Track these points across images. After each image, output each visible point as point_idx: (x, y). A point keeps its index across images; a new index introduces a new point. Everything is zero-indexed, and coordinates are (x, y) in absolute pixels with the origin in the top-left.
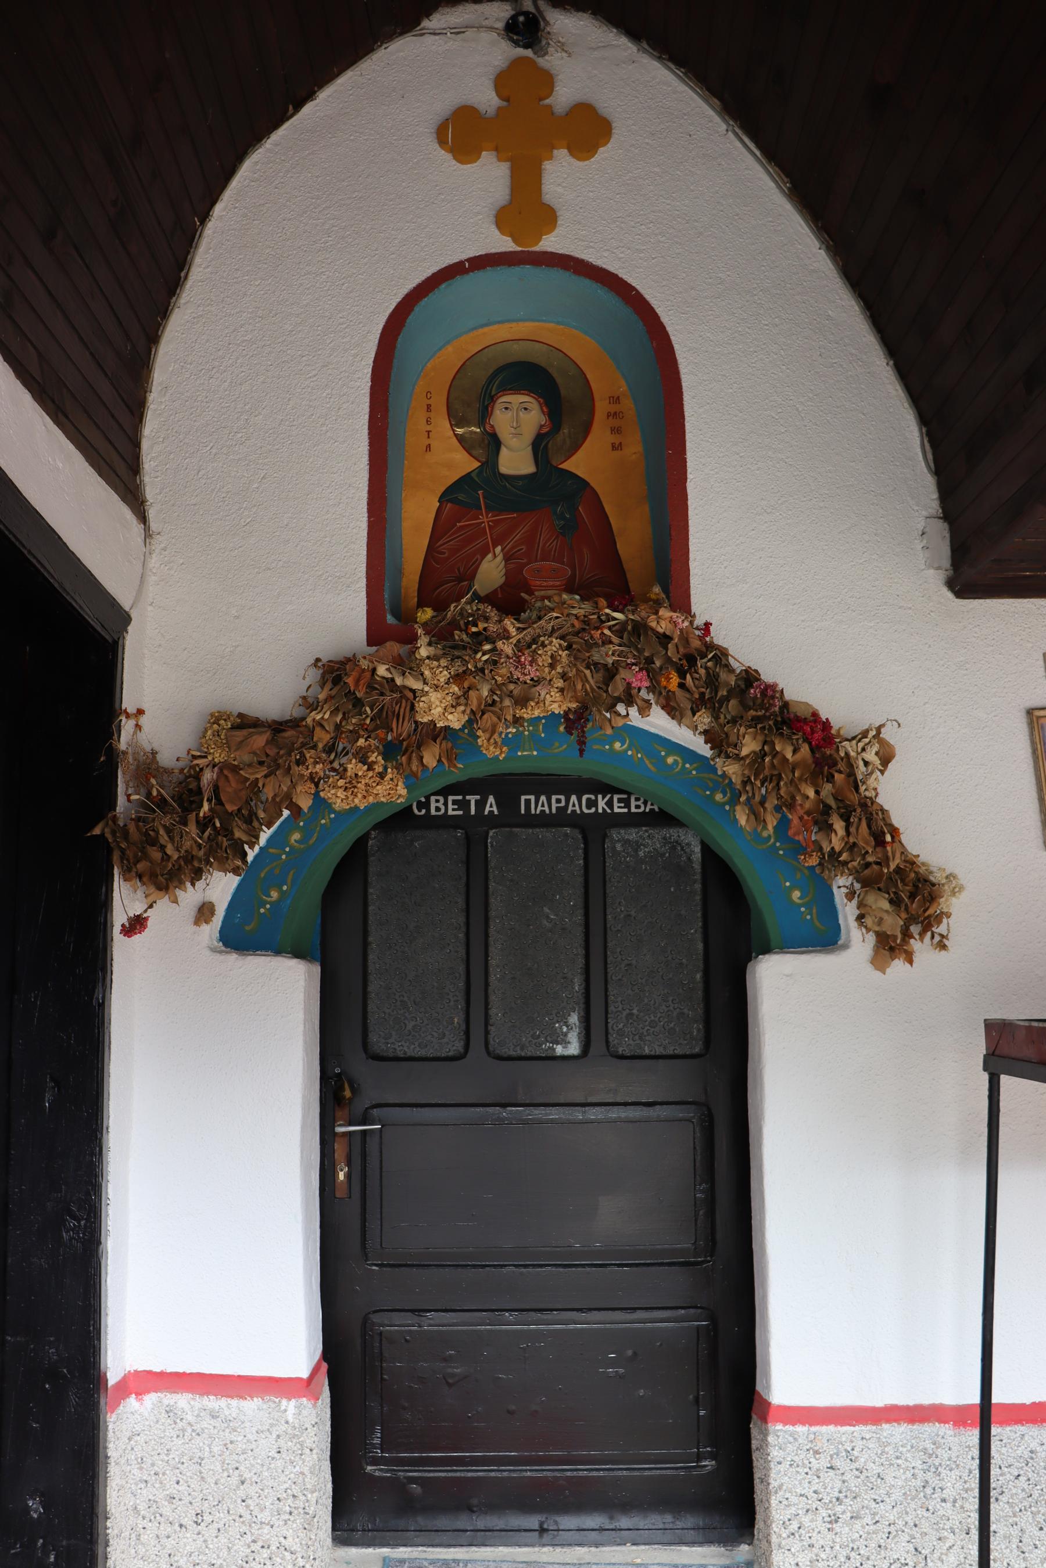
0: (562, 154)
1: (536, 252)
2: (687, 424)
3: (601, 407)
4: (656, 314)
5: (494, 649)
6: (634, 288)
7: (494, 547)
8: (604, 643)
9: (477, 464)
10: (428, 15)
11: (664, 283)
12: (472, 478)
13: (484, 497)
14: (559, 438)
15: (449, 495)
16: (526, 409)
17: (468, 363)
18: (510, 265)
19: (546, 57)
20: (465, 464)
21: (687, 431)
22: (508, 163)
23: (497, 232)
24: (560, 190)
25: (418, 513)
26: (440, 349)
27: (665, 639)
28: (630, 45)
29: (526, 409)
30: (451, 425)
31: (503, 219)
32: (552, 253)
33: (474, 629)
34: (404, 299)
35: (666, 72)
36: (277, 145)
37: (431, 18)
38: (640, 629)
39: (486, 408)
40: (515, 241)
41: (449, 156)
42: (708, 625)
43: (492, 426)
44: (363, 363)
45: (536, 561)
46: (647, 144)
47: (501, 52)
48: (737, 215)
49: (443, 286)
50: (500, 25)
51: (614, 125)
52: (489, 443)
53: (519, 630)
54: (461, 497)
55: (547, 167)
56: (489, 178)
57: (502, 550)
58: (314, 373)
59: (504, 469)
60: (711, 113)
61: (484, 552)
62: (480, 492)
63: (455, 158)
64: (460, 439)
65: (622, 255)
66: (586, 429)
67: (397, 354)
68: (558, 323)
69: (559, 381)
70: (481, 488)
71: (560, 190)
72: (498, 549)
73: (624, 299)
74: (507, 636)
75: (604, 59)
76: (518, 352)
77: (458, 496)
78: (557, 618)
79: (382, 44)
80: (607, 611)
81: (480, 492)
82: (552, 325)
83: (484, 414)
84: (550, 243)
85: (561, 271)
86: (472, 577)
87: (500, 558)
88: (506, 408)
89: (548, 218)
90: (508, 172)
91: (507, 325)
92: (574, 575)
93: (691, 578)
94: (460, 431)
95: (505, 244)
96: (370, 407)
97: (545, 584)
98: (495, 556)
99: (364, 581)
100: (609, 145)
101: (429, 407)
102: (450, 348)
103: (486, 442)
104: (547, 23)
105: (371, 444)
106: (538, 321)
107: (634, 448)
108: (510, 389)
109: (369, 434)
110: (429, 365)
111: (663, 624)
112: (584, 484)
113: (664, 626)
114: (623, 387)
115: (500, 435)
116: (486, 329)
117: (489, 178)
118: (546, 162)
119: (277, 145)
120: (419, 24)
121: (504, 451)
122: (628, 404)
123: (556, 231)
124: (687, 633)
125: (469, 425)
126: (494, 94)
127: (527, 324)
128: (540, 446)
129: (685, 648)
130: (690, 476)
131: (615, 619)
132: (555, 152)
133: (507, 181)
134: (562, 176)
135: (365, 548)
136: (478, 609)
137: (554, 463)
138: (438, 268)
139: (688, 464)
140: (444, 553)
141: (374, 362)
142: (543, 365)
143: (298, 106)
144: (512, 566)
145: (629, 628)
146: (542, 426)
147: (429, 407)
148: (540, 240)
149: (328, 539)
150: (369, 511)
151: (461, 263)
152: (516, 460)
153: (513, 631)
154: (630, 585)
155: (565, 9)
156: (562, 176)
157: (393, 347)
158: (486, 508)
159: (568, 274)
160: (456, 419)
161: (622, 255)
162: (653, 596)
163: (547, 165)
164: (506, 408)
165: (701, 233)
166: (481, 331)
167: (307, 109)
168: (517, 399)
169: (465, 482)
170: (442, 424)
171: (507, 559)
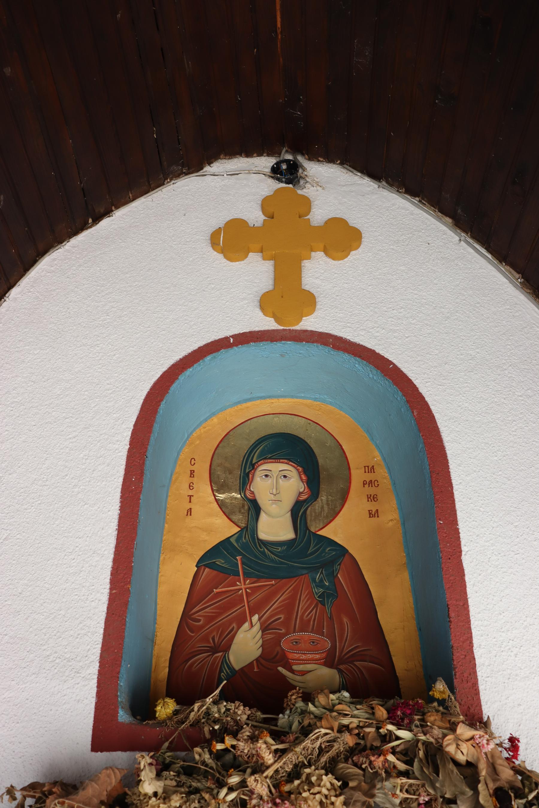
0: (319, 256)
1: (296, 331)
2: (455, 493)
3: (357, 476)
4: (415, 386)
5: (243, 784)
6: (391, 363)
7: (251, 615)
8: (389, 774)
9: (237, 529)
10: (210, 164)
11: (419, 358)
12: (231, 544)
13: (243, 563)
14: (317, 505)
15: (207, 560)
16: (285, 477)
17: (231, 433)
18: (272, 341)
19: (304, 190)
20: (225, 529)
21: (457, 500)
22: (272, 262)
23: (261, 314)
24: (318, 282)
25: (174, 578)
26: (206, 420)
27: (469, 771)
28: (372, 183)
29: (285, 477)
30: (213, 490)
31: (266, 303)
32: (312, 331)
33: (220, 747)
34: (170, 368)
35: (404, 201)
36: (74, 247)
37: (212, 165)
38: (435, 756)
39: (247, 475)
40: (278, 321)
41: (220, 256)
42: (513, 740)
43: (253, 493)
44: (124, 426)
45: (294, 632)
46: (393, 249)
47: (270, 186)
48: (478, 303)
49: (208, 358)
50: (268, 170)
51: (363, 235)
52: (249, 509)
53: (279, 754)
54: (220, 562)
55: (306, 264)
56: (256, 273)
57: (260, 619)
58: (74, 434)
59: (263, 535)
60: (444, 228)
61: (241, 620)
62: (238, 558)
63: (226, 257)
64: (221, 504)
65: (378, 334)
66: (344, 496)
67: (158, 418)
68: (315, 399)
69: (316, 451)
70: (240, 554)
71: (318, 282)
72: (256, 618)
73: (382, 372)
74: (259, 768)
75: (352, 192)
76: (280, 425)
77: (216, 560)
78: (326, 734)
79: (171, 180)
80: (390, 727)
81: (238, 558)
82: (309, 401)
83: (245, 480)
84: (309, 323)
85: (321, 347)
86: (227, 648)
87: (257, 627)
88: (266, 476)
89: (308, 302)
90: (272, 268)
91: (269, 401)
92: (334, 647)
93: (478, 669)
94: (221, 496)
95: (268, 324)
96: (126, 470)
97: (304, 657)
98: (252, 626)
99: (96, 666)
100: (360, 250)
101: (192, 472)
102: (215, 420)
103: (246, 507)
104: (304, 169)
105: (122, 508)
106: (297, 397)
107: (391, 514)
108: (270, 458)
109: (122, 497)
110: (195, 434)
111: (465, 747)
112: (342, 551)
113: (465, 752)
114: (377, 457)
115: (260, 502)
116: (249, 404)
117: (256, 273)
118: (305, 261)
119: (74, 247)
120: (202, 169)
121: (263, 516)
122: (382, 474)
123: (315, 314)
124: (493, 756)
125: (230, 490)
126: (261, 213)
127: (287, 400)
128: (298, 512)
129: (494, 780)
130: (464, 549)
131: (398, 738)
132: (313, 254)
133: (271, 275)
134: (318, 272)
135: (102, 625)
136: (228, 710)
137: (313, 529)
138: (204, 343)
139: (461, 535)
140: (199, 621)
141: (135, 426)
142: (302, 436)
143: (97, 219)
144: (269, 637)
145: (421, 753)
146: (300, 493)
147: (192, 472)
148: (300, 320)
149: (62, 612)
150: (112, 582)
151: (227, 339)
152: (276, 527)
153: (269, 758)
154: (394, 658)
155: (319, 161)
156: (318, 272)
157: (155, 412)
158: (244, 573)
159: (327, 349)
160: (217, 484)
161: (378, 334)
162: (437, 695)
163: (306, 264)
164: (266, 476)
165: (448, 318)
166: (244, 405)
167: (105, 223)
168: (276, 468)
169: (223, 548)
170: (204, 490)
171: (264, 629)
